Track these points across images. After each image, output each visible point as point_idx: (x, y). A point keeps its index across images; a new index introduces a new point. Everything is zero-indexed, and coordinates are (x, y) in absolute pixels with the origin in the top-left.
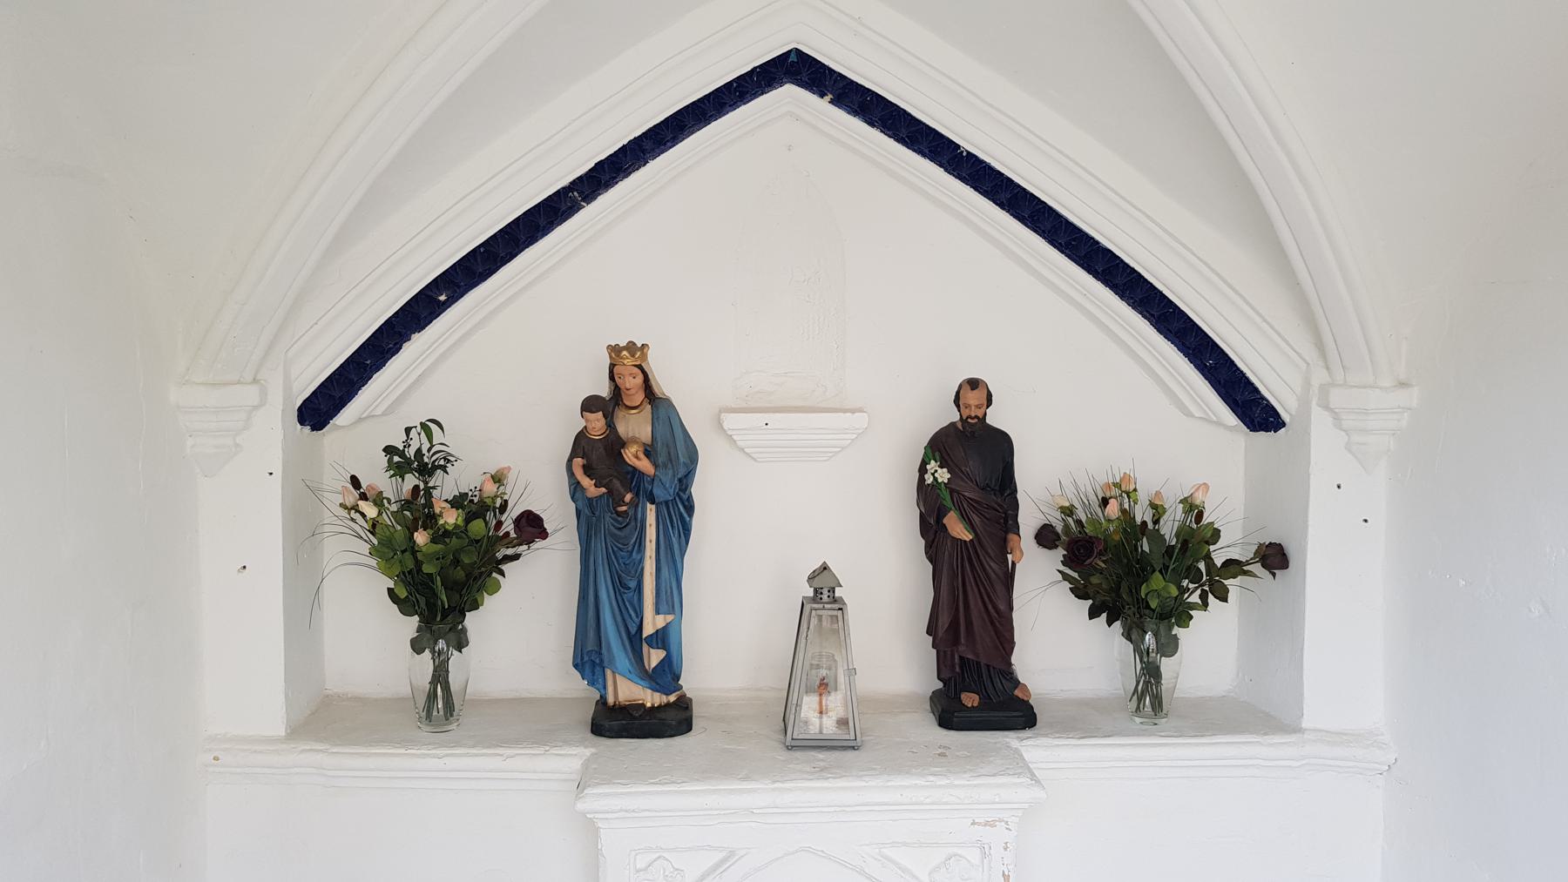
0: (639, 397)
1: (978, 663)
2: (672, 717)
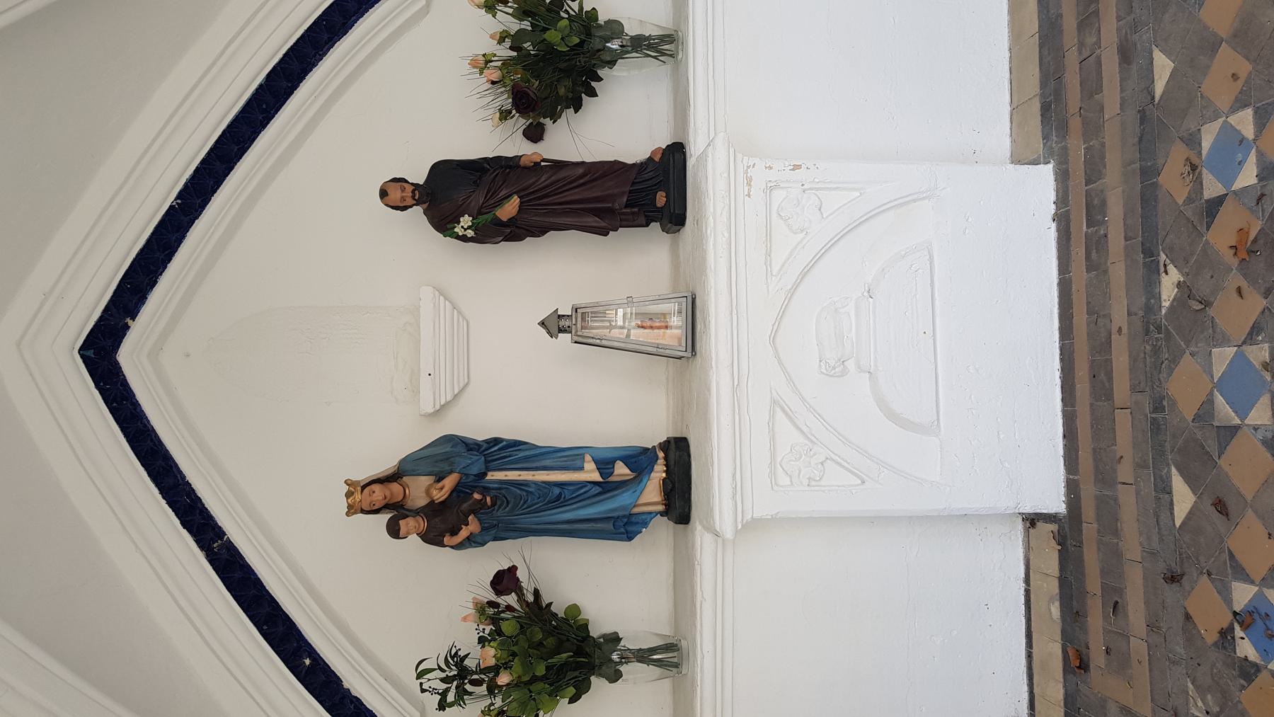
0: (395, 487)
1: (630, 192)
2: (673, 455)
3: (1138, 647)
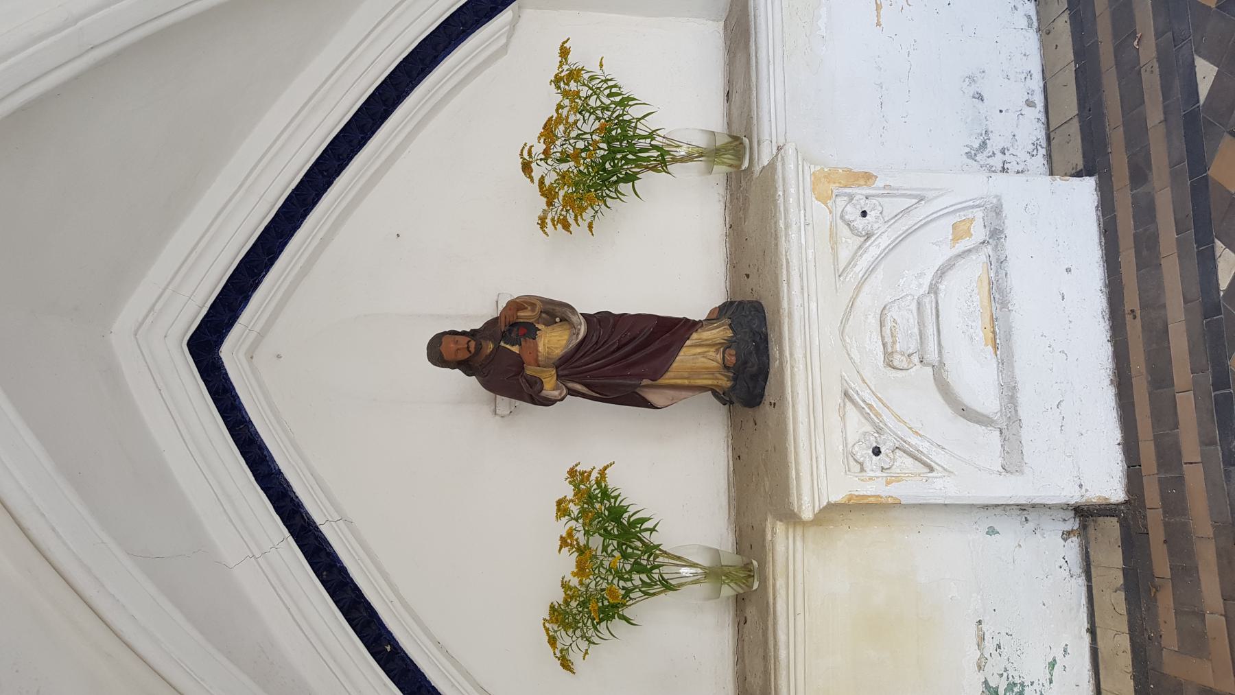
3: (1216, 623)
